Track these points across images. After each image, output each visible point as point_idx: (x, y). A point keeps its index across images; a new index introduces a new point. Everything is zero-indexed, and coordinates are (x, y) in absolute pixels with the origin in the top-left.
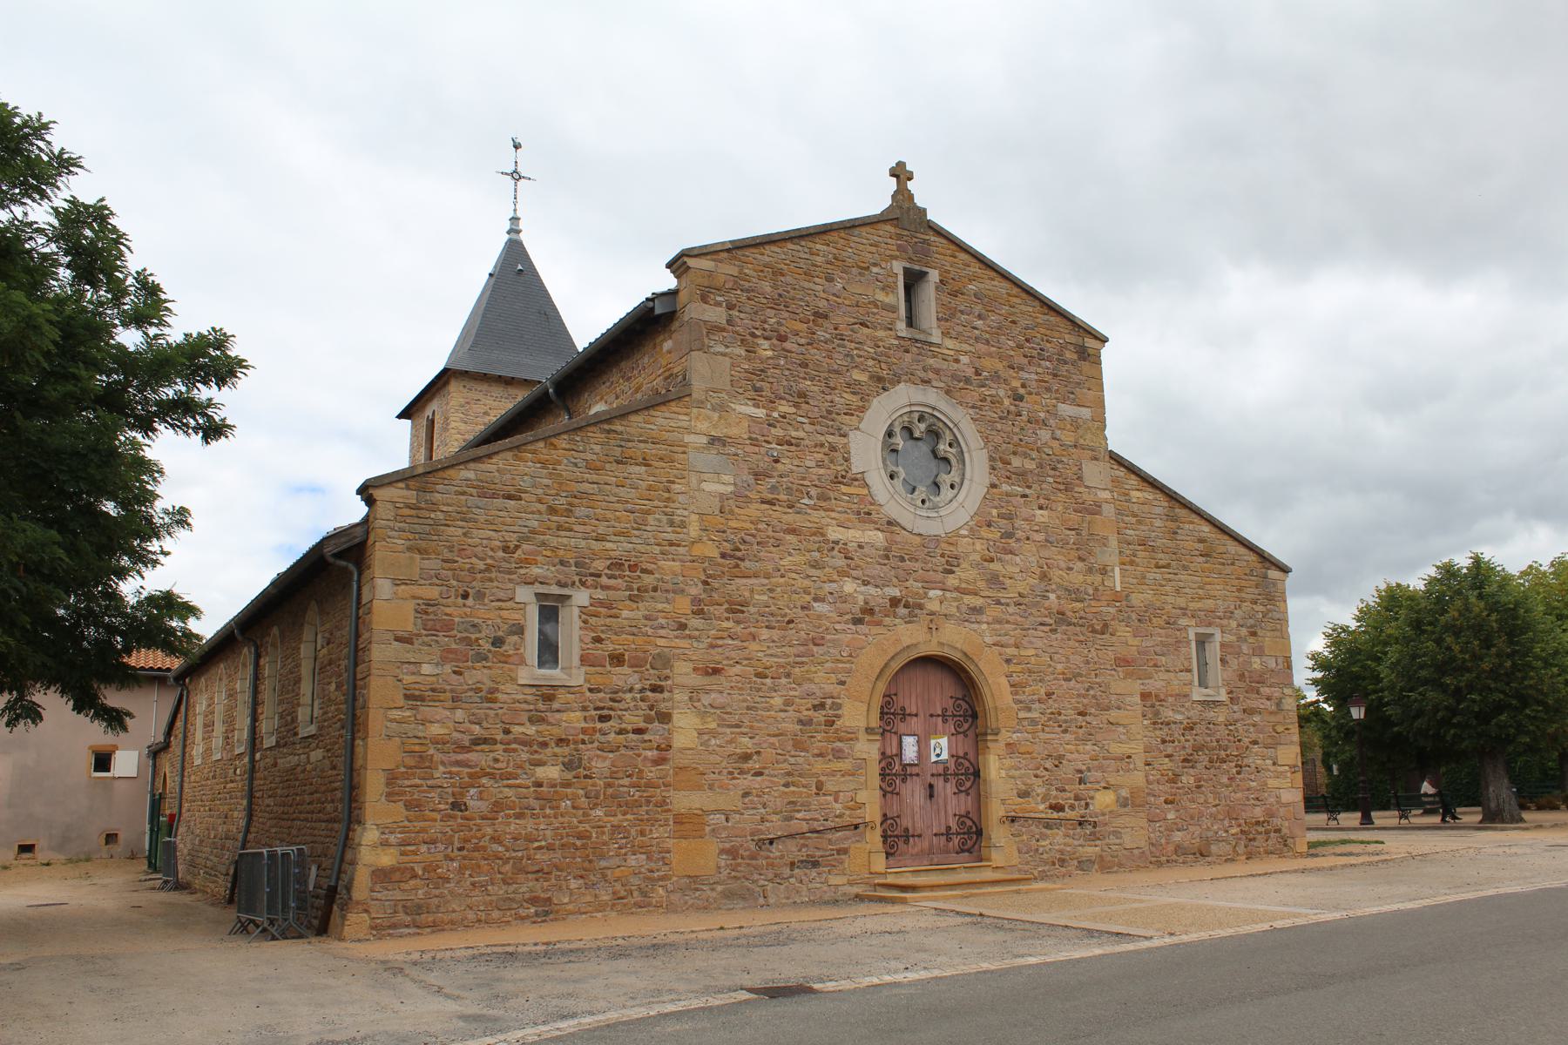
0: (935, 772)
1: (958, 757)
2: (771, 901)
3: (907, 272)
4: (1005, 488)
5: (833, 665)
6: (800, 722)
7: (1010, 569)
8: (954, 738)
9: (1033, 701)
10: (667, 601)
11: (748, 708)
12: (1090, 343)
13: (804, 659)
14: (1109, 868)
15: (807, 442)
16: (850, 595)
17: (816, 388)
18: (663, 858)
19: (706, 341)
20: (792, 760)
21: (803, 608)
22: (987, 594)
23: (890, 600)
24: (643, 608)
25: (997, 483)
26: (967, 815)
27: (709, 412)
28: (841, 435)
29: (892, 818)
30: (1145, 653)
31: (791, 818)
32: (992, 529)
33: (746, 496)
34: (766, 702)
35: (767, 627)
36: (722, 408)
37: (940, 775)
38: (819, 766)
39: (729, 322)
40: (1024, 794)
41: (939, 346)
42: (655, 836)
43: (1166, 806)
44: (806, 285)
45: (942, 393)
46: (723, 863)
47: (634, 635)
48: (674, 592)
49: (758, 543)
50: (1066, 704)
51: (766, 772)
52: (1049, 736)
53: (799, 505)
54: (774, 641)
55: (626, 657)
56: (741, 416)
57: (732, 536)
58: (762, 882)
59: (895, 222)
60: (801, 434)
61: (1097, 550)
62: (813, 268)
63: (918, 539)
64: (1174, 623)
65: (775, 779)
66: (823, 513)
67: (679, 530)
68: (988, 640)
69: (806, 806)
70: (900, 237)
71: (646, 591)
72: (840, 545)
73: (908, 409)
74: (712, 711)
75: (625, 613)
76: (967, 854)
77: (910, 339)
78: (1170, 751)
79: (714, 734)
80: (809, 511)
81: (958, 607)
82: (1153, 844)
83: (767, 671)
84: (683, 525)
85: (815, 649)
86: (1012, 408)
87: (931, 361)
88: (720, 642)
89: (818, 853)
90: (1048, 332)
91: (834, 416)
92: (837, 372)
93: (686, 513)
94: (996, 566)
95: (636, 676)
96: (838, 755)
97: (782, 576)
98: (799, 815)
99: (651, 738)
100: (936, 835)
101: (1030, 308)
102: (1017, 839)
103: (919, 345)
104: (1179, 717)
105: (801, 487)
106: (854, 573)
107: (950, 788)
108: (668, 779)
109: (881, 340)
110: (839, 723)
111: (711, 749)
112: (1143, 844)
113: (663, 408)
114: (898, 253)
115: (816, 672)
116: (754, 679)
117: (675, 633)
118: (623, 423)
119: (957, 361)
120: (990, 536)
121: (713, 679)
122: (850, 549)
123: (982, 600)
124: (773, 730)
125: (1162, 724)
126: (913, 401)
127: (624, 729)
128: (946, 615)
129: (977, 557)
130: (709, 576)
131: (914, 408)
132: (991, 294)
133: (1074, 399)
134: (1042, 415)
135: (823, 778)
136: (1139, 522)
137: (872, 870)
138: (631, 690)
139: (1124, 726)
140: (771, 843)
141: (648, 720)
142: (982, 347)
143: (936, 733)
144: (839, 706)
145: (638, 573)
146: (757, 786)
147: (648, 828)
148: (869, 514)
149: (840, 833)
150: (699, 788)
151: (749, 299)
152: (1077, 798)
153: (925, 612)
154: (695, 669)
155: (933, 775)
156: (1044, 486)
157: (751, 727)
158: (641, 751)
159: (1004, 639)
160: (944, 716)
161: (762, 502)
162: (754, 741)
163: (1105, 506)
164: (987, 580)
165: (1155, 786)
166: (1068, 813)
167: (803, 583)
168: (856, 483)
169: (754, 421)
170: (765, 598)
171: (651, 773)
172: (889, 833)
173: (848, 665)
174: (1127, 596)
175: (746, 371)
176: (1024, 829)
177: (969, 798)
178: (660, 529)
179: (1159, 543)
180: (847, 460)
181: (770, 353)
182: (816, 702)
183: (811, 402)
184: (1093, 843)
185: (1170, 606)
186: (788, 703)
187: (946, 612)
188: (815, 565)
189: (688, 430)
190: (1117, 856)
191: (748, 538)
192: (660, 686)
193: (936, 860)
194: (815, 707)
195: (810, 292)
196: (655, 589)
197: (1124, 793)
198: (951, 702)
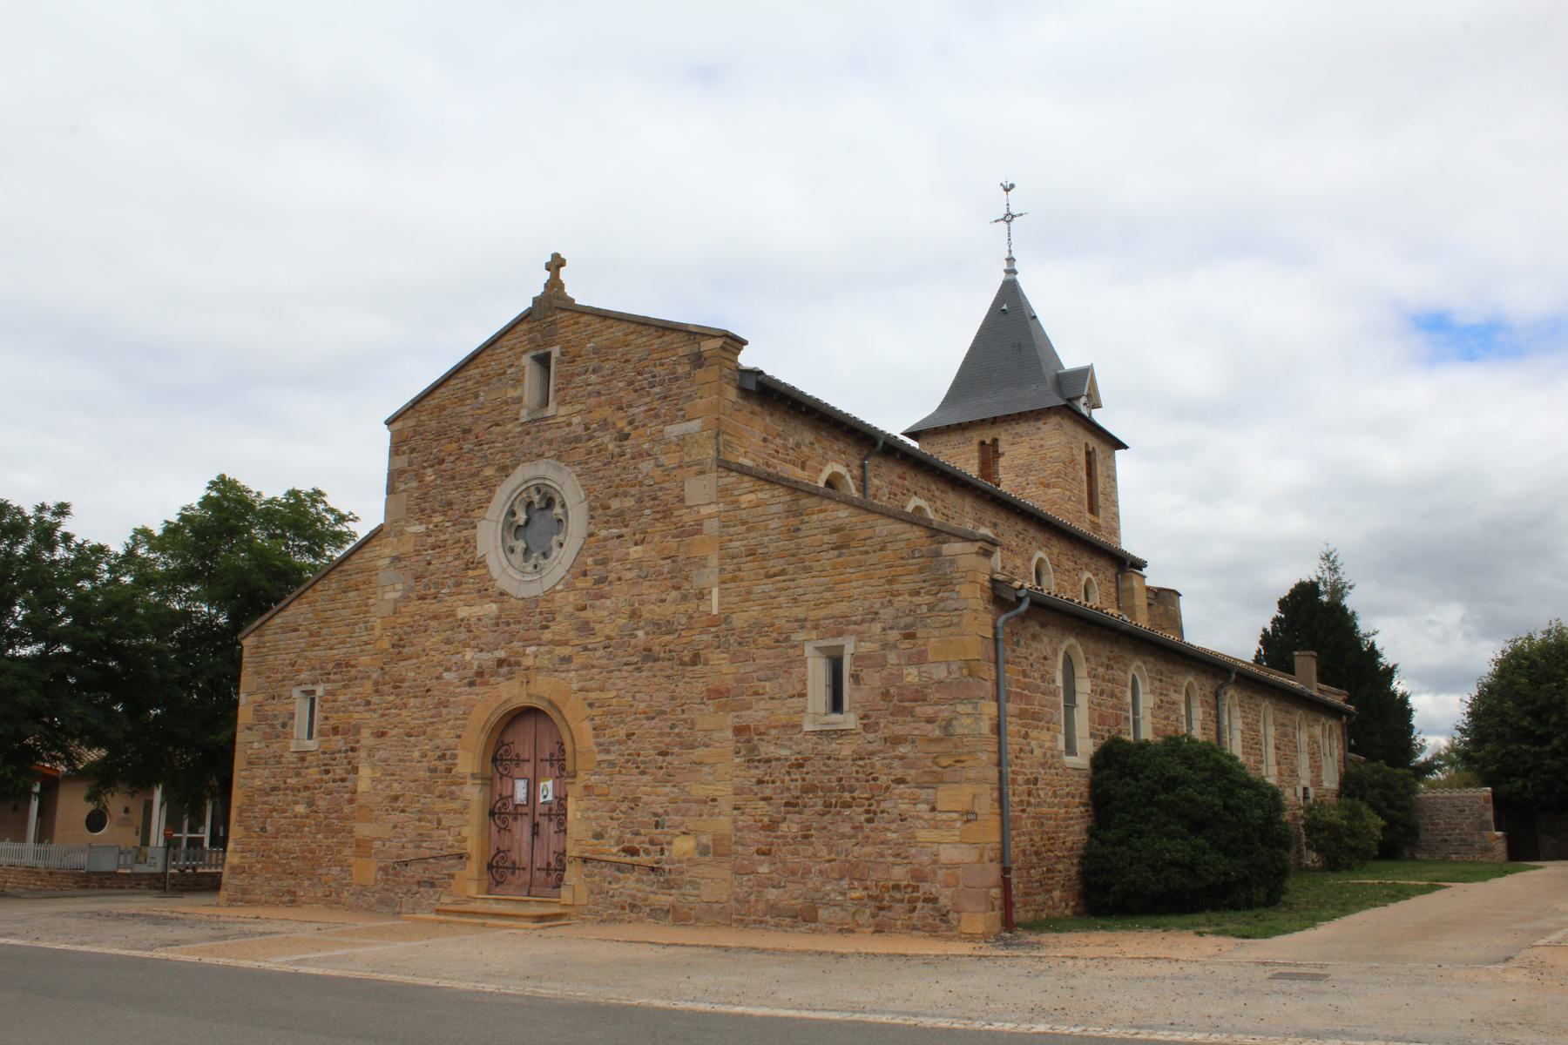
3: (537, 359)
4: (603, 533)
8: (558, 780)
9: (611, 744)
11: (400, 761)
20: (422, 800)
21: (437, 678)
22: (577, 642)
30: (742, 680)
38: (439, 805)
39: (410, 464)
51: (407, 809)
59: (529, 318)
63: (521, 603)
78: (768, 792)
96: (453, 797)
100: (539, 869)
102: (588, 880)
106: (473, 643)
113: (369, 545)
119: (569, 424)
125: (759, 761)
129: (569, 609)
130: (385, 663)
133: (684, 416)
134: (646, 446)
135: (441, 815)
136: (749, 530)
142: (593, 401)
148: (486, 590)
150: (370, 821)
152: (652, 842)
154: (372, 734)
155: (541, 815)
160: (551, 760)
163: (706, 523)
166: (643, 859)
167: (438, 657)
173: (462, 722)
176: (596, 871)
179: (772, 547)
180: (475, 548)
185: (784, 621)
186: (424, 755)
188: (448, 642)
197: (706, 839)
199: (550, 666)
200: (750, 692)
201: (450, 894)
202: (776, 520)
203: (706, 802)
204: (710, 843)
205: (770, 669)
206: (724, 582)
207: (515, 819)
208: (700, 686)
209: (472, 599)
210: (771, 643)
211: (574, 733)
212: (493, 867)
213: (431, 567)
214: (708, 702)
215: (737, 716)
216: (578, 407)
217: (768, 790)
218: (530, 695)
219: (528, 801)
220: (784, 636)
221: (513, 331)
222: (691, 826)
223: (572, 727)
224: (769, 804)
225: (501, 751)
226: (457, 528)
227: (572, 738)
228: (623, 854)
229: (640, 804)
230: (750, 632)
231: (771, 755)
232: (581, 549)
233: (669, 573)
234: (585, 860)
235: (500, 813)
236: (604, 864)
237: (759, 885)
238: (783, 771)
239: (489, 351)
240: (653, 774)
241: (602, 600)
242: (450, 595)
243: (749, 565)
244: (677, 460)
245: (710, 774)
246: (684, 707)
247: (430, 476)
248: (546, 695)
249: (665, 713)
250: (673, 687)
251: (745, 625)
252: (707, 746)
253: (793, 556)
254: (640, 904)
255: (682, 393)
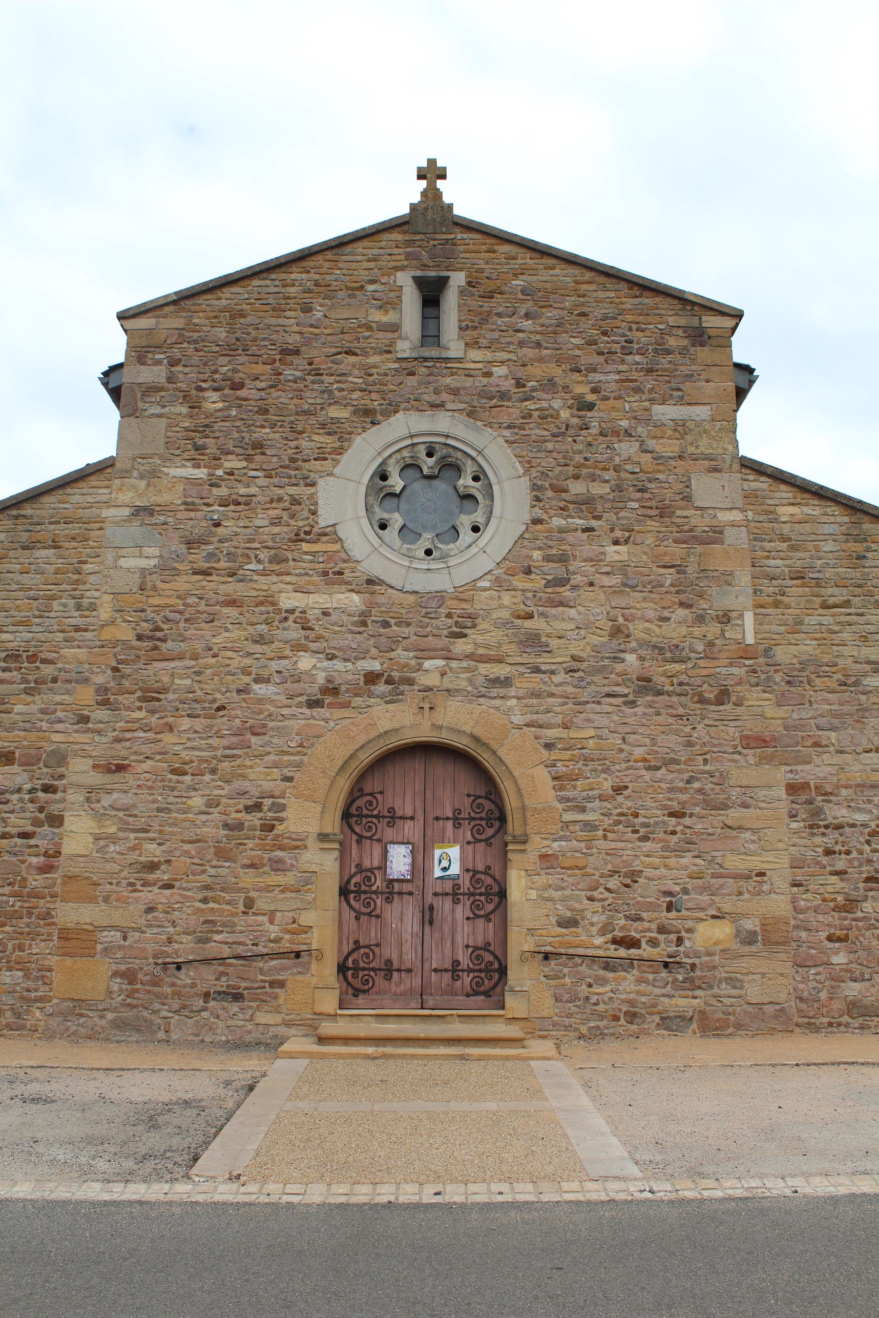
0: (439, 890)
1: (475, 872)
2: (174, 1037)
3: (419, 282)
4: (557, 522)
5: (276, 758)
6: (226, 826)
7: (559, 625)
8: (470, 848)
9: (589, 799)
10: (68, 692)
11: (159, 810)
12: (710, 321)
13: (235, 752)
14: (717, 1029)
15: (260, 498)
16: (307, 673)
17: (277, 436)
18: (43, 977)
19: (140, 405)
20: (213, 871)
21: (239, 691)
22: (519, 660)
23: (365, 675)
24: (39, 702)
25: (545, 517)
26: (486, 947)
27: (135, 481)
28: (307, 485)
29: (368, 947)
30: (796, 728)
31: (208, 940)
32: (533, 576)
33: (174, 569)
34: (185, 803)
35: (189, 716)
36: (153, 475)
37: (447, 894)
38: (249, 879)
39: (170, 380)
40: (568, 922)
41: (459, 360)
42: (34, 951)
43: (830, 945)
44: (273, 321)
45: (463, 417)
46: (116, 988)
47: (26, 730)
48: (77, 682)
49: (187, 620)
50: (649, 803)
51: (177, 884)
52: (613, 845)
53: (241, 572)
54: (196, 732)
55: (17, 755)
56: (174, 480)
57: (153, 615)
58: (164, 1013)
59: (405, 228)
60: (253, 490)
61: (714, 591)
62: (283, 302)
63: (412, 598)
64: (856, 684)
65: (189, 894)
66: (274, 578)
67: (87, 613)
68: (517, 719)
69: (230, 927)
70: (409, 243)
71: (44, 682)
72: (297, 614)
73: (408, 442)
74: (114, 813)
75: (18, 708)
76: (482, 997)
77: (416, 359)
78: (840, 865)
79: (112, 839)
80: (255, 578)
81: (470, 681)
82: (801, 999)
83: (186, 767)
84: (93, 607)
85: (253, 739)
86: (575, 421)
87: (448, 380)
88: (128, 735)
89: (243, 984)
90: (640, 319)
91: (300, 463)
92: (306, 413)
93: (97, 594)
94: (536, 624)
95: (25, 775)
96: (278, 866)
97: (215, 656)
98: (217, 937)
99: (39, 843)
101: (611, 292)
102: (553, 983)
103: (429, 364)
104: (860, 817)
105: (247, 551)
106: (313, 646)
107: (462, 911)
108: (55, 889)
109: (375, 366)
110: (279, 829)
111: (108, 856)
112: (782, 997)
113: (81, 484)
114: (406, 263)
115: (251, 767)
116: (170, 776)
117: (76, 727)
118: (35, 506)
119: (488, 374)
120: (529, 586)
121: (117, 777)
122: (311, 617)
123: (508, 668)
124: (190, 835)
125: (826, 827)
126: (414, 431)
127: (8, 833)
128: (448, 690)
129: (505, 614)
130: (120, 662)
131: (416, 440)
132: (548, 286)
133: (682, 398)
134: (624, 423)
135: (253, 894)
136: (793, 548)
137: (317, 1010)
138: (19, 790)
139: (754, 831)
140: (179, 968)
141: (37, 823)
142: (528, 352)
143: (443, 840)
144: (283, 808)
145: (38, 664)
146: (165, 901)
147: (27, 943)
148: (340, 573)
149: (275, 962)
150: (92, 900)
151: (197, 350)
152: (662, 930)
153: (416, 687)
154: (95, 767)
156: (623, 514)
157: (161, 832)
158: (27, 857)
159: (542, 718)
160: (455, 819)
161: (194, 573)
162: (163, 848)
163: (728, 531)
164: (521, 642)
165: (811, 916)
166: (646, 951)
167: (238, 661)
168: (324, 539)
169: (192, 484)
170: (188, 682)
171: (36, 881)
172: (362, 964)
173: (297, 758)
174: (767, 651)
175: (186, 429)
176: (566, 970)
177: (491, 925)
178: (66, 615)
179: (829, 573)
180: (314, 513)
181: (220, 405)
182: (249, 803)
183: (268, 452)
184: (690, 993)
185: (850, 660)
186: (212, 803)
188: (260, 640)
189: (108, 504)
190: (734, 1013)
191: (172, 616)
192: (51, 786)
193: (431, 1003)
194: (248, 809)
195: (278, 328)
196: (55, 680)
197: (749, 925)
198: (467, 801)
199: (470, 689)
200: (810, 742)
201: (277, 1010)
202: (830, 542)
203: (749, 877)
204: (758, 929)
205: (835, 716)
206: (762, 607)
207: (389, 900)
208: (732, 731)
209: (310, 583)
210: (835, 686)
211: (519, 781)
212: (349, 969)
213: (220, 530)
214: (745, 751)
215: (791, 771)
216: (504, 356)
217: (841, 863)
218: (435, 727)
219: (413, 874)
220: (854, 679)
221: (376, 238)
222: (727, 908)
223: (516, 774)
224: (842, 880)
225: (360, 802)
226: (276, 480)
227: (519, 790)
228: (613, 946)
229: (641, 880)
230: (802, 670)
231: (845, 820)
232: (521, 537)
233: (672, 585)
234: (547, 956)
235: (359, 892)
236: (578, 960)
237: (833, 979)
238: (862, 839)
239: (329, 255)
240: (661, 841)
241: (560, 609)
242: (264, 573)
243: (796, 592)
244: (677, 449)
245: (754, 841)
246: (708, 757)
247: (213, 402)
248: (467, 729)
249: (677, 762)
250: (688, 729)
251: (795, 661)
252: (744, 805)
253: (859, 586)
254: (643, 1011)
255: (676, 370)
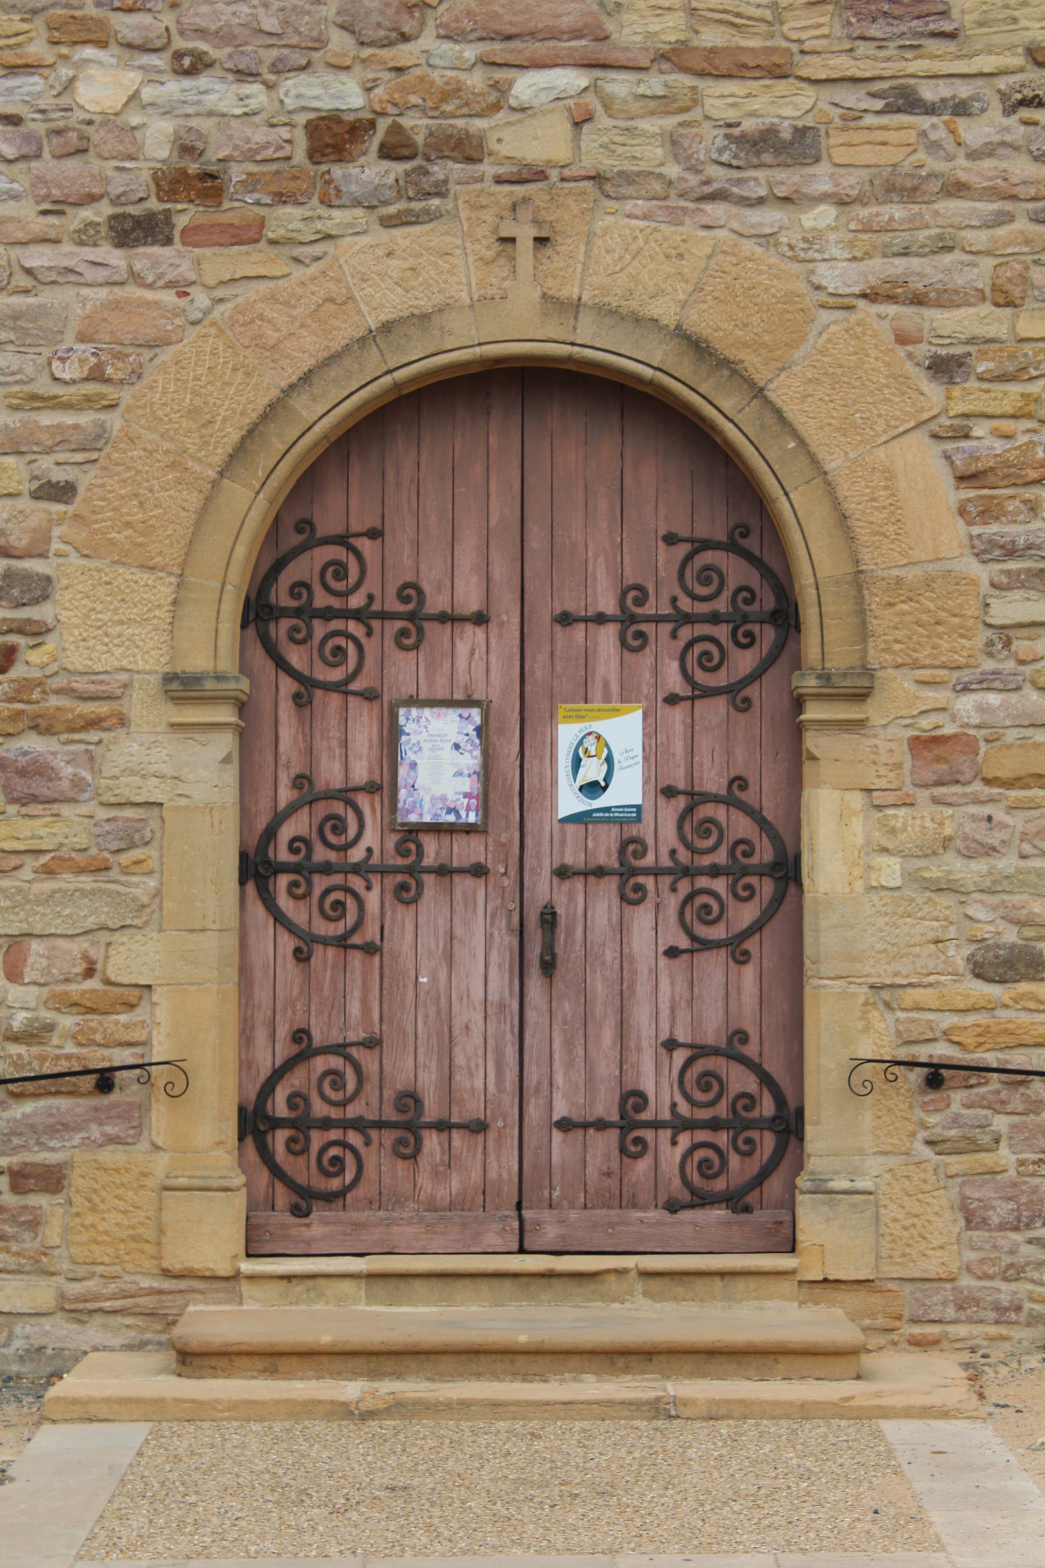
0: (573, 858)
1: (696, 798)
8: (678, 715)
16: (109, 121)
22: (844, 66)
29: (339, 1049)
37: (600, 872)
76: (720, 1213)
81: (673, 142)
100: (565, 1125)
102: (956, 1163)
128: (597, 178)
137: (174, 1263)
149: (28, 1107)
153: (488, 169)
155: (562, 873)
160: (627, 619)
173: (85, 419)
176: (1001, 1123)
177: (749, 974)
187: (607, 164)
193: (550, 1233)
198: (667, 559)
199: (673, 171)
211: (844, 490)
219: (485, 801)
223: (834, 462)
248: (666, 311)
